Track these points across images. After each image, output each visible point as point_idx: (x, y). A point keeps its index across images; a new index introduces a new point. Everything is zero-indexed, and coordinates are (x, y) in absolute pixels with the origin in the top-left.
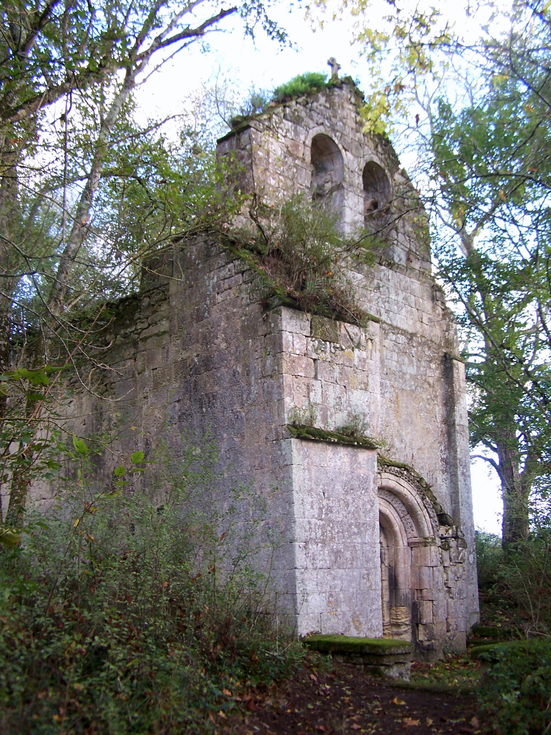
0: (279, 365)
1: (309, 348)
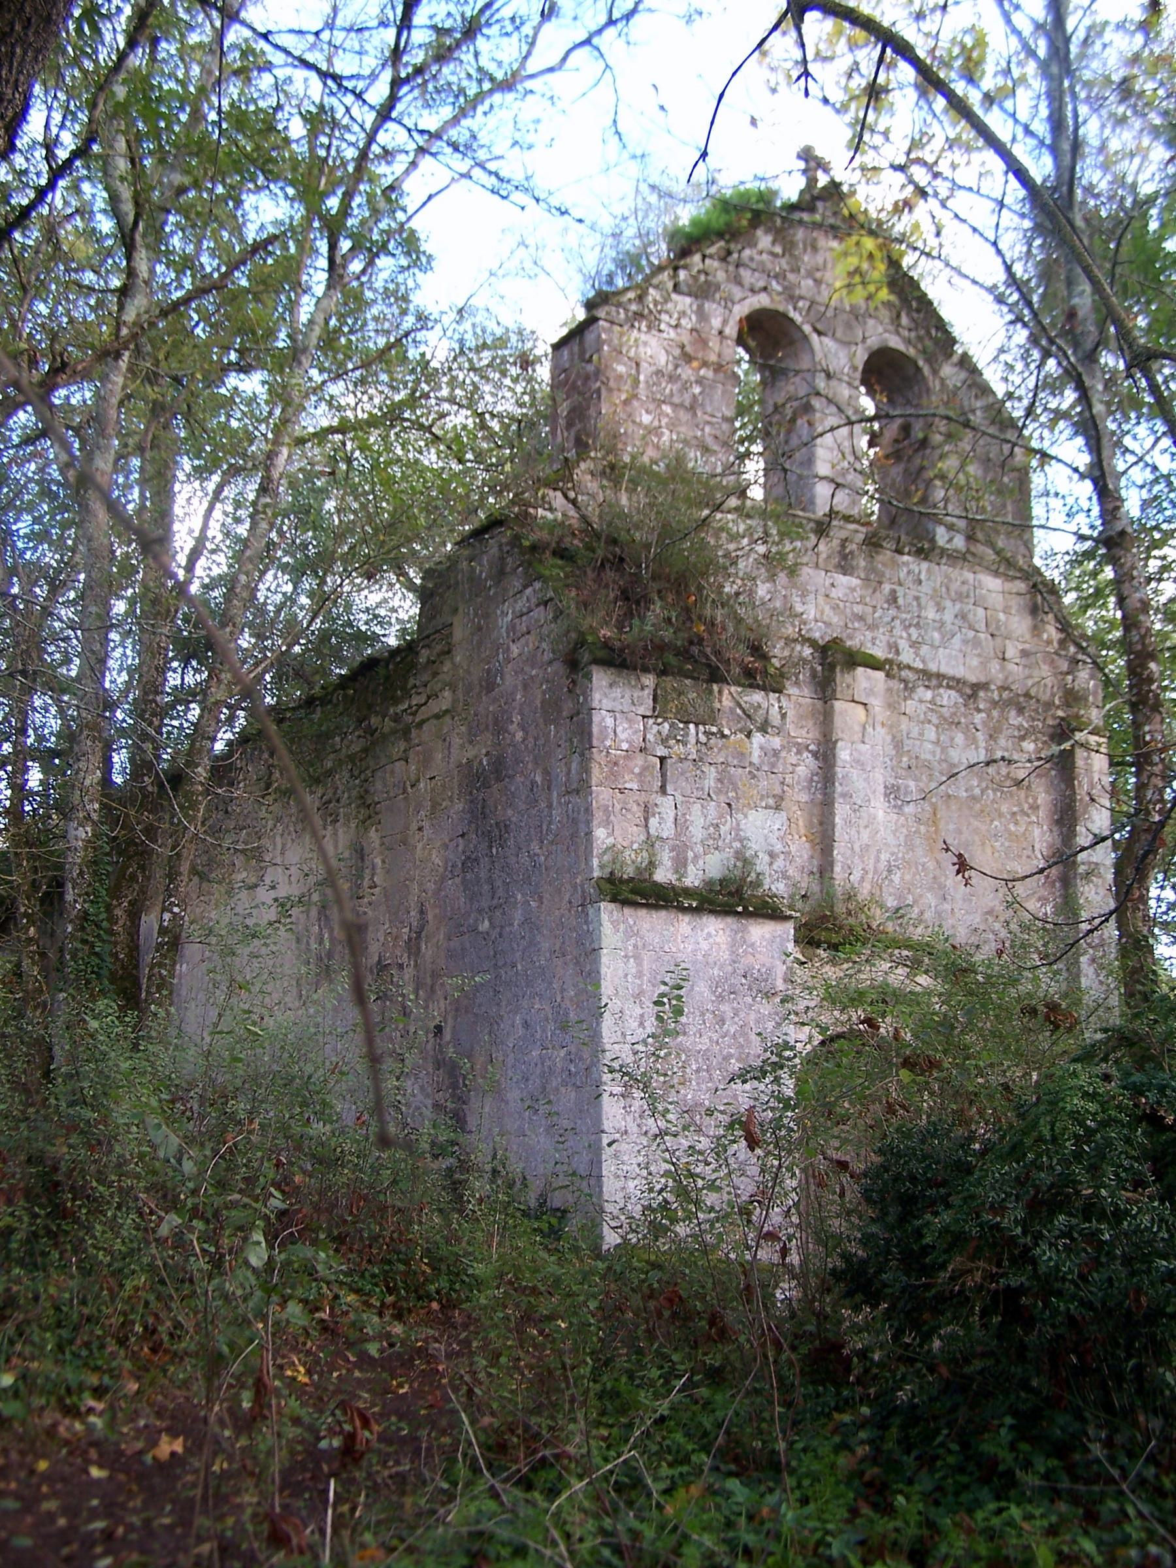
0: (588, 771)
1: (650, 737)
